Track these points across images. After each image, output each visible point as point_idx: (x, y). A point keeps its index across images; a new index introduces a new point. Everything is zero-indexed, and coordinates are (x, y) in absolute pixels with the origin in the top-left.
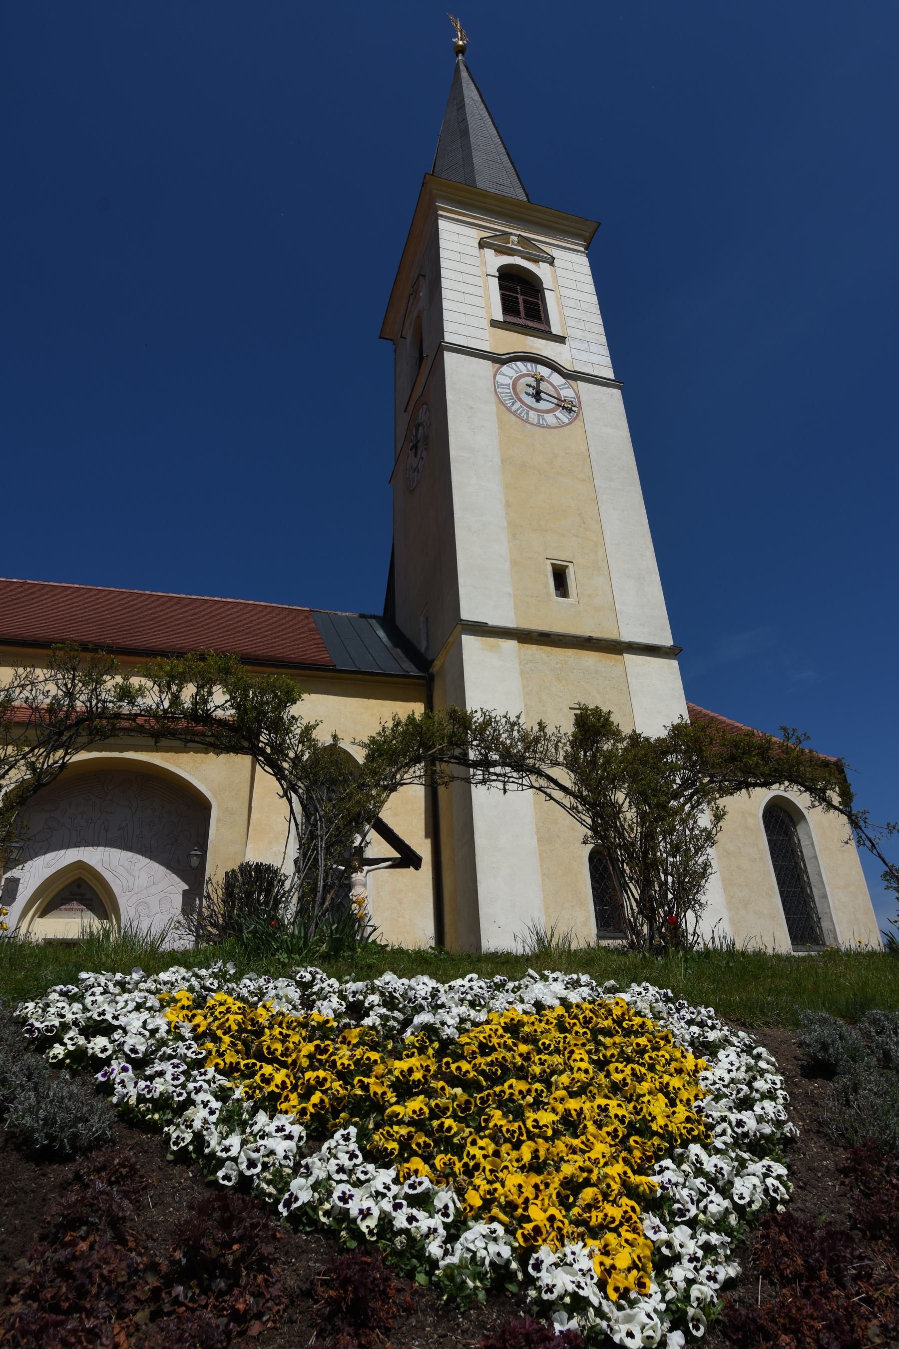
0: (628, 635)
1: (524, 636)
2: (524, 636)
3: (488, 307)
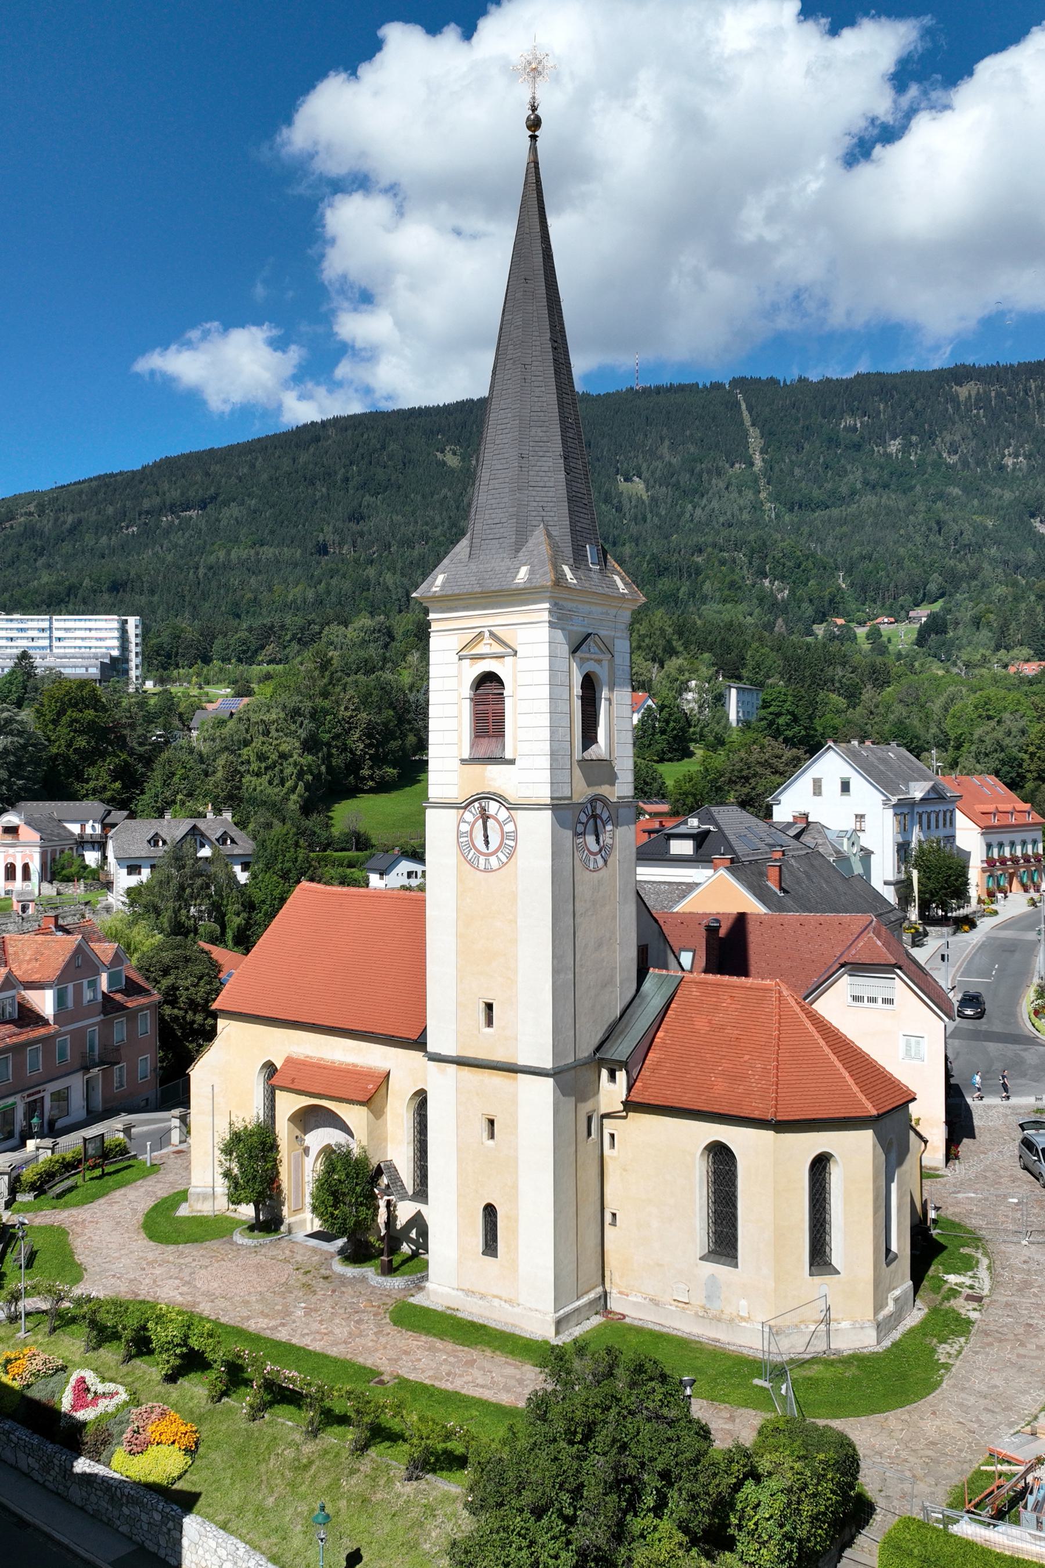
0: (522, 1061)
1: (461, 1062)
2: (461, 1062)
3: (460, 748)
